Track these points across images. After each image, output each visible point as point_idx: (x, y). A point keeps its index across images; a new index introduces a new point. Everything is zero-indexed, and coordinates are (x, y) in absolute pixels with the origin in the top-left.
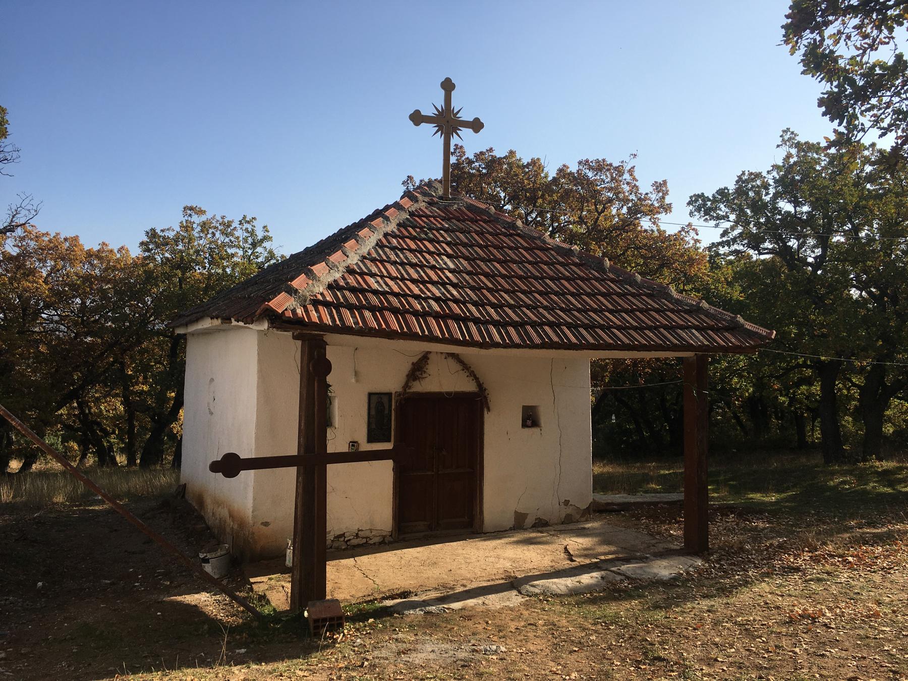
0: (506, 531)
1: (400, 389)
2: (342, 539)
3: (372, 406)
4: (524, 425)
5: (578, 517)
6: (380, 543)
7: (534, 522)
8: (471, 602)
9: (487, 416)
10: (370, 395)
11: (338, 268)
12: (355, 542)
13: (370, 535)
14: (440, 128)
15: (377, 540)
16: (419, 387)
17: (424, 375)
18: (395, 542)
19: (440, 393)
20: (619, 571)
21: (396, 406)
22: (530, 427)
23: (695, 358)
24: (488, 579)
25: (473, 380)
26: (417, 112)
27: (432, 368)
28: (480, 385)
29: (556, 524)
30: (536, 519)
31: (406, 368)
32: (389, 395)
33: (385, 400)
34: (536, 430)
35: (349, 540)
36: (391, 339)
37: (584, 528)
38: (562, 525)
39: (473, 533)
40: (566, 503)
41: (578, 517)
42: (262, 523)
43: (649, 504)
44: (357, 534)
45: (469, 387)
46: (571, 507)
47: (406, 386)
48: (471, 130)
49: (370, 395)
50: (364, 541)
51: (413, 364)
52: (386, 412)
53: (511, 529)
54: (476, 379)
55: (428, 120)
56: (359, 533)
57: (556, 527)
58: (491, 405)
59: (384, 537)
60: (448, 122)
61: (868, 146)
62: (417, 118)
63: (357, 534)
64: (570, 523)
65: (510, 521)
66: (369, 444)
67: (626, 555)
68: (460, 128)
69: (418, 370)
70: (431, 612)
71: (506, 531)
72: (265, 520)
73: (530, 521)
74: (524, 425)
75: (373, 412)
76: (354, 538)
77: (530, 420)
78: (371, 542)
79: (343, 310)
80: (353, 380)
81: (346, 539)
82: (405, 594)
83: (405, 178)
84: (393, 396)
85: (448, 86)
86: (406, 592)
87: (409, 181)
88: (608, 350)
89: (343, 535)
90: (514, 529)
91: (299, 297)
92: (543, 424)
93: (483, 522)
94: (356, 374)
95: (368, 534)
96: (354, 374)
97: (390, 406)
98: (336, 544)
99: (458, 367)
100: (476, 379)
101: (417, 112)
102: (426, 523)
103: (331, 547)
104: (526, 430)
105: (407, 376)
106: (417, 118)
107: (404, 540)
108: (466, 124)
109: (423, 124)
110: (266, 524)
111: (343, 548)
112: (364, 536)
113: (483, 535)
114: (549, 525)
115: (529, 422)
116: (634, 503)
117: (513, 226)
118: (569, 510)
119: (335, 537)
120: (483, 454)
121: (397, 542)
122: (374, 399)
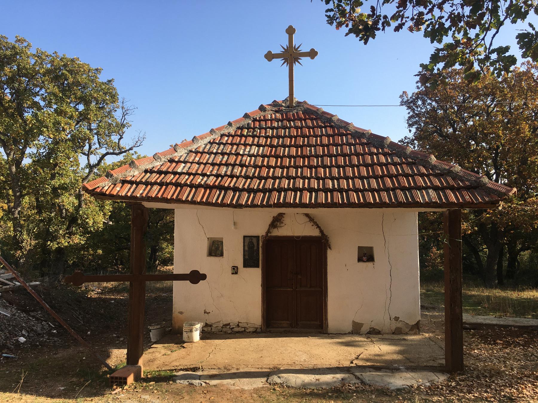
0: (345, 334)
1: (264, 234)
2: (228, 327)
3: (245, 244)
4: (360, 260)
5: (407, 330)
6: (253, 332)
7: (368, 330)
8: (225, 382)
9: (329, 252)
10: (245, 237)
11: (161, 159)
12: (236, 329)
13: (247, 326)
14: (286, 60)
15: (251, 330)
16: (277, 233)
17: (282, 225)
18: (262, 332)
19: (292, 237)
20: (360, 376)
21: (263, 245)
22: (365, 262)
23: (448, 212)
24: (258, 367)
25: (317, 228)
26: (270, 52)
27: (287, 220)
28: (321, 231)
29: (388, 334)
30: (370, 328)
31: (269, 220)
32: (258, 237)
33: (255, 240)
34: (370, 264)
35: (233, 328)
36: (169, 203)
37: (405, 339)
38: (393, 335)
39: (320, 333)
40: (397, 319)
41: (407, 330)
42: (179, 312)
43: (500, 326)
44: (238, 325)
45: (315, 233)
46: (401, 323)
47: (268, 232)
48: (309, 58)
49: (245, 237)
50: (243, 329)
51: (274, 217)
52: (255, 248)
53: (349, 333)
54: (318, 227)
55: (277, 56)
56: (240, 324)
57: (386, 336)
58: (332, 246)
59: (257, 328)
60: (291, 55)
61: (371, 13)
62: (270, 56)
63: (238, 325)
64: (399, 334)
65: (350, 328)
66: (245, 269)
67: (384, 365)
68: (300, 58)
69: (277, 221)
70: (193, 384)
71: (345, 334)
72: (181, 311)
73: (365, 329)
74: (360, 260)
75: (246, 248)
76: (236, 327)
77: (365, 257)
78: (247, 331)
79: (431, 177)
80: (233, 228)
81: (231, 327)
82: (195, 369)
83: (401, 93)
84: (260, 238)
85: (291, 31)
86: (196, 368)
87: (404, 95)
88: (341, 207)
89: (229, 324)
90: (352, 334)
91: (113, 179)
92: (375, 260)
93: (328, 326)
94: (235, 224)
95: (245, 325)
96: (233, 224)
97: (258, 244)
98: (224, 330)
99: (307, 219)
100: (318, 227)
101: (270, 52)
102: (288, 322)
103: (221, 331)
104: (361, 264)
105: (269, 225)
106: (270, 56)
107: (270, 332)
108: (277, 56)
109: (274, 60)
110: (181, 313)
111: (229, 332)
112: (243, 326)
113: (327, 335)
114: (380, 334)
115: (365, 258)
116: (486, 324)
117: (330, 120)
118: (399, 325)
119: (224, 325)
120: (327, 279)
121: (265, 333)
122: (247, 240)
